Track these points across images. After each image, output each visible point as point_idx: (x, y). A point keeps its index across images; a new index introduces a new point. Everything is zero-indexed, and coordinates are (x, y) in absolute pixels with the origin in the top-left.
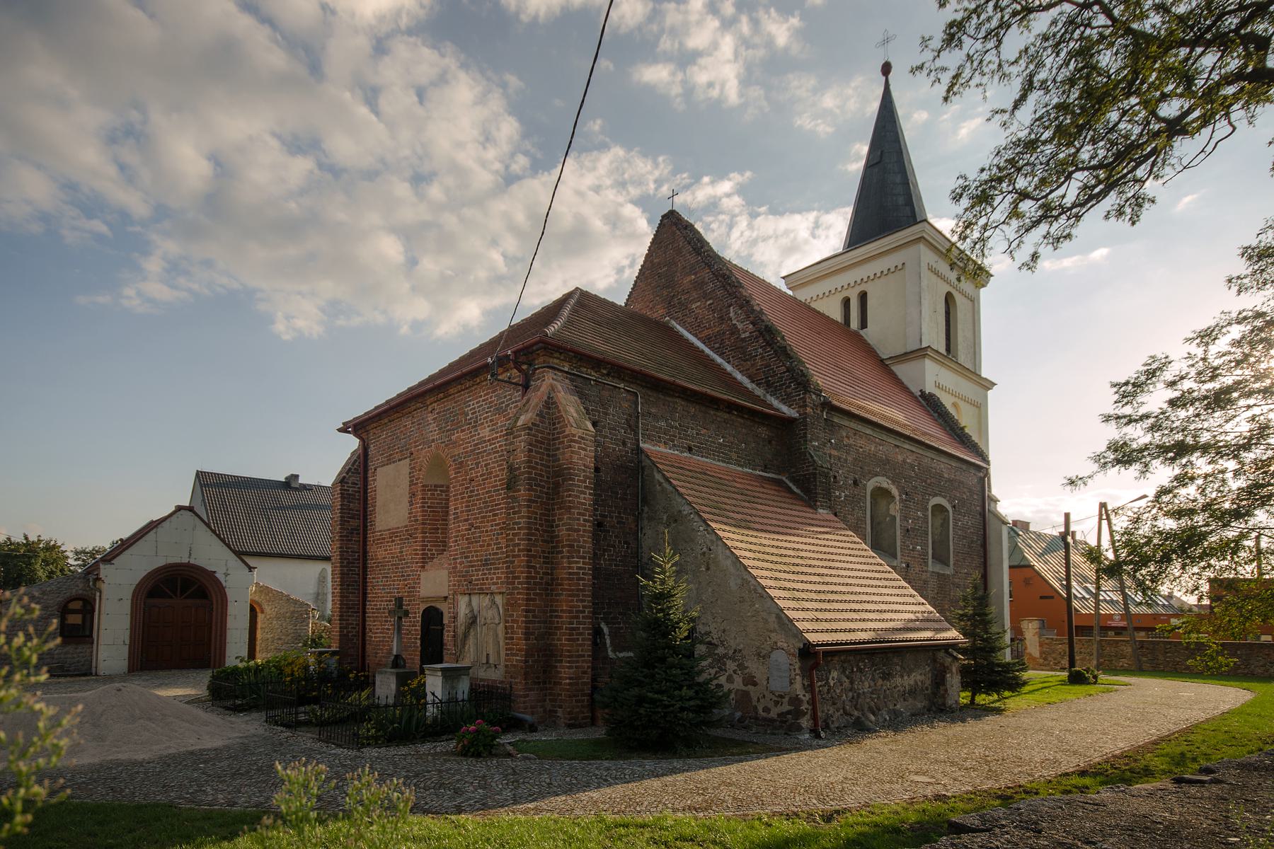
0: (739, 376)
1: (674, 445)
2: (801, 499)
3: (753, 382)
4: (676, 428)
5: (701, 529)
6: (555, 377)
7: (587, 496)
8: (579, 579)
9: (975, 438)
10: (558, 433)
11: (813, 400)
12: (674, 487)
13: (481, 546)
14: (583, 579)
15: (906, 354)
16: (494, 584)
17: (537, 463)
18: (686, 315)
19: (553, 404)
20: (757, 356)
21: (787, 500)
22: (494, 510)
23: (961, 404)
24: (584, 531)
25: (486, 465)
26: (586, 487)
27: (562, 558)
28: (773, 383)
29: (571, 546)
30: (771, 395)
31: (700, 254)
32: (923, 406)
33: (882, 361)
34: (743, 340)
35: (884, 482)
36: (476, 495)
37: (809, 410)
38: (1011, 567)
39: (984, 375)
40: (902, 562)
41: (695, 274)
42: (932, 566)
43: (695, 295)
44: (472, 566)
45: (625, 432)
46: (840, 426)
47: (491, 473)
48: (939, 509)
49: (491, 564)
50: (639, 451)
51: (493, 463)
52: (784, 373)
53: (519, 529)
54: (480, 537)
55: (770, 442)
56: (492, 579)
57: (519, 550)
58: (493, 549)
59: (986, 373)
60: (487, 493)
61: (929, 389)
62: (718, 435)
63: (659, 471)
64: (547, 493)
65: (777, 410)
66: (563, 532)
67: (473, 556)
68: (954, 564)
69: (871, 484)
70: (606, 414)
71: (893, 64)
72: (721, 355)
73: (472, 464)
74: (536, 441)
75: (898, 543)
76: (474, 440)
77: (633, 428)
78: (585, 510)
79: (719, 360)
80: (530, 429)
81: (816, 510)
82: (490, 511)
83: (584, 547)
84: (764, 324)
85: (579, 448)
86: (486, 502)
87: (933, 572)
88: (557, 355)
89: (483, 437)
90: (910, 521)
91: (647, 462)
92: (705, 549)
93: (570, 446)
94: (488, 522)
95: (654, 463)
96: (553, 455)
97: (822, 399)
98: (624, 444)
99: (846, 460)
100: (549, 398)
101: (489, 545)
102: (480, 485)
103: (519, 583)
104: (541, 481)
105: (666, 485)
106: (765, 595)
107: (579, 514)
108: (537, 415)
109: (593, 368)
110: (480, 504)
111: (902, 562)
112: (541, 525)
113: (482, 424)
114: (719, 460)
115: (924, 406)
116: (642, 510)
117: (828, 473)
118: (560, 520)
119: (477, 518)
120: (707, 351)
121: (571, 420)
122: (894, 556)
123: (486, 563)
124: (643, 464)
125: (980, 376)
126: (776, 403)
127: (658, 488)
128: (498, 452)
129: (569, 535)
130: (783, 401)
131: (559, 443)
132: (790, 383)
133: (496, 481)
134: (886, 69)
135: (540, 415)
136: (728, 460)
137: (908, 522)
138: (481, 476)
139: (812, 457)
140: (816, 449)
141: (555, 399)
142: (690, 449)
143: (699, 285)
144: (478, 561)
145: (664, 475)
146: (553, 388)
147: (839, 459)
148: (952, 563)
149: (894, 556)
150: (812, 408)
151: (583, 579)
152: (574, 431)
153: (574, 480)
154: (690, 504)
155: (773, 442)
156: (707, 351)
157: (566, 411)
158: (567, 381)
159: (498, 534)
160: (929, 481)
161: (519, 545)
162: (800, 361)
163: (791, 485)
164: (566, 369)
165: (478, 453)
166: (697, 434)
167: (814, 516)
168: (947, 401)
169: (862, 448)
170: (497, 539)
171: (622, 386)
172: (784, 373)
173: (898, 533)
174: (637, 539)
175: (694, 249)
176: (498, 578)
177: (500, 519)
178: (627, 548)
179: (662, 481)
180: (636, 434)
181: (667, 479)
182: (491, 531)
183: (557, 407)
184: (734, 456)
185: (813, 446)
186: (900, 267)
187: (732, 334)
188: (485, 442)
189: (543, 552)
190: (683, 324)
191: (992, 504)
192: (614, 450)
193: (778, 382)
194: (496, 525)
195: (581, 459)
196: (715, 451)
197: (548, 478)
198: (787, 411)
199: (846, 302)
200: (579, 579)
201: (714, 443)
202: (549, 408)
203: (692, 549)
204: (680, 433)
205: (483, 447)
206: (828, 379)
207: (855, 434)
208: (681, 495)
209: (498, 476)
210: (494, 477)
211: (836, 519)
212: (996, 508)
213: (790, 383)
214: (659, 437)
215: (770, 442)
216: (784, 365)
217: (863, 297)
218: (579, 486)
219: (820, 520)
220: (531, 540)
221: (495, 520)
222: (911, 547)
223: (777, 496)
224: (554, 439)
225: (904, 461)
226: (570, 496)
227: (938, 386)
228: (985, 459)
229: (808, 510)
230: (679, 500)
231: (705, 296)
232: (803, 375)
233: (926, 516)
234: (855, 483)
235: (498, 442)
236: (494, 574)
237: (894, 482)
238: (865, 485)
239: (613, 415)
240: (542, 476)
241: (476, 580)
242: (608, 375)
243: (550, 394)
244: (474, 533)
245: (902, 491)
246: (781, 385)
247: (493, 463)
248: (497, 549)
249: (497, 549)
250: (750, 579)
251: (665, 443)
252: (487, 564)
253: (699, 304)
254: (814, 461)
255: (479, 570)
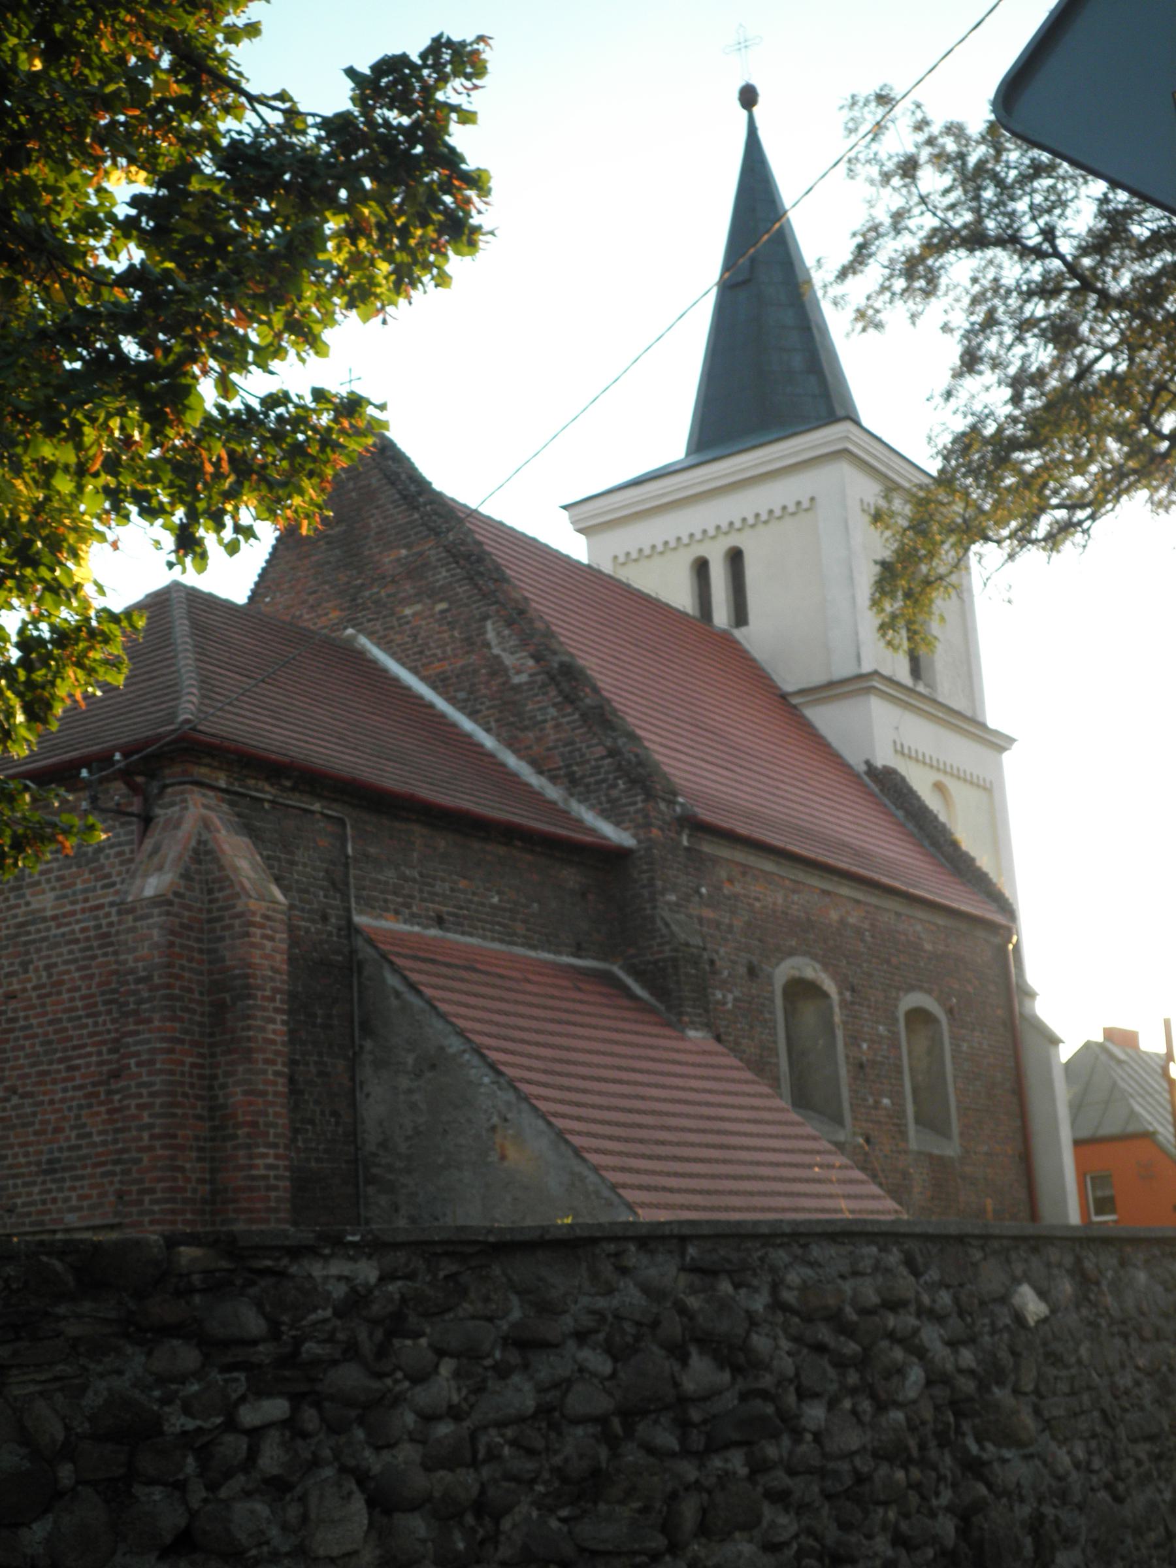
0: (511, 761)
1: (413, 915)
2: (652, 1010)
3: (541, 772)
4: (414, 880)
5: (486, 1080)
6: (205, 801)
7: (279, 1027)
8: (270, 1188)
9: (984, 862)
10: (220, 909)
11: (661, 812)
12: (429, 1002)
13: (36, 1133)
14: (276, 1188)
15: (831, 685)
16: (72, 1210)
17: (182, 968)
18: (392, 628)
19: (207, 853)
20: (545, 721)
21: (627, 1014)
22: (70, 1058)
23: (952, 785)
24: (276, 1094)
25: (48, 967)
26: (277, 1010)
27: (235, 1148)
28: (583, 777)
29: (254, 1124)
30: (580, 801)
31: (416, 508)
32: (872, 794)
33: (784, 697)
34: (517, 688)
35: (811, 970)
36: (23, 1028)
37: (655, 833)
38: (1077, 1143)
39: (991, 724)
40: (854, 1134)
41: (408, 546)
42: (915, 1138)
43: (408, 588)
44: (15, 1176)
45: (326, 896)
46: (715, 860)
47: (61, 983)
48: (919, 1016)
49: (64, 1169)
50: (351, 929)
51: (66, 962)
52: (602, 758)
53: (152, 1095)
54: (34, 1114)
55: (583, 895)
56: (67, 1200)
57: (153, 1137)
58: (68, 1139)
59: (994, 720)
60: (51, 1022)
61: (884, 758)
62: (489, 890)
63: (396, 970)
64: (200, 1024)
65: (592, 831)
66: (237, 1095)
67: (15, 1156)
68: (962, 1134)
69: (785, 971)
70: (292, 863)
71: (760, 90)
72: (472, 715)
73: (11, 964)
74: (182, 925)
75: (845, 1094)
76: (15, 916)
77: (338, 885)
78: (277, 1053)
79: (467, 725)
80: (170, 903)
81: (682, 1031)
82: (60, 1061)
83: (275, 1125)
84: (557, 658)
85: (265, 937)
86: (50, 1042)
87: (919, 1153)
88: (207, 760)
89: (39, 911)
90: (865, 1046)
91: (367, 952)
92: (495, 1120)
93: (247, 934)
94: (54, 1082)
95: (384, 956)
96: (209, 951)
97: (678, 809)
98: (325, 918)
99: (730, 926)
100: (199, 842)
101: (58, 1130)
102: (33, 1007)
103: (153, 1202)
104: (191, 1000)
105: (411, 997)
106: (616, 1200)
107: (267, 1061)
108: (182, 876)
109: (267, 779)
110: (33, 1045)
111: (854, 1134)
112: (192, 1086)
113: (38, 883)
114: (493, 939)
115: (872, 794)
116: (361, 1047)
117: (700, 956)
118: (227, 1074)
119: (28, 1076)
120: (441, 704)
121: (247, 885)
122: (839, 1121)
123: (51, 1168)
124: (360, 956)
125: (983, 726)
126: (590, 818)
127: (394, 1002)
128: (77, 941)
129: (250, 1103)
130: (605, 814)
131: (224, 928)
132: (616, 778)
133: (72, 999)
134: (748, 97)
135: (186, 876)
136: (508, 937)
137: (859, 1046)
138: (35, 988)
139: (667, 925)
140: (675, 907)
141: (211, 845)
142: (440, 921)
143: (415, 570)
144: (29, 1164)
145: (405, 979)
146: (206, 824)
147: (718, 925)
148: (955, 1129)
149: (839, 1121)
150: (661, 829)
151: (276, 1188)
152: (253, 905)
153: (254, 997)
154: (461, 1033)
155: (591, 897)
156: (441, 704)
157: (236, 869)
158: (225, 807)
159: (80, 1107)
160: (894, 960)
161: (150, 1126)
162: (633, 737)
163: (630, 981)
164: (222, 784)
165: (26, 943)
166: (452, 890)
167: (681, 1045)
168: (920, 782)
169: (757, 899)
170: (78, 1117)
171: (317, 807)
172: (602, 758)
173: (843, 1072)
174: (353, 1105)
175: (405, 497)
176: (81, 1198)
177: (84, 1076)
178: (337, 1124)
179: (402, 988)
180: (345, 898)
181: (413, 987)
182: (63, 1100)
183: (217, 860)
184: (520, 928)
185: (668, 903)
186: (806, 504)
187: (493, 674)
188: (44, 920)
189: (197, 1138)
190: (385, 644)
191: (1027, 1002)
192: (307, 931)
193: (592, 775)
194: (75, 1088)
195: (266, 957)
196: (485, 921)
197: (201, 994)
198: (611, 832)
199: (701, 568)
200: (270, 1188)
201: (483, 905)
202: (199, 862)
203: (469, 1121)
204: (421, 891)
205: (38, 931)
206: (683, 757)
207: (744, 874)
208: (442, 1016)
209: (78, 989)
210: (69, 991)
211: (719, 1048)
212: (1033, 1009)
213: (616, 778)
214: (386, 901)
215: (583, 895)
216: (601, 743)
217: (735, 558)
218: (264, 1009)
219: (691, 1052)
220: (174, 1115)
221: (73, 1079)
222: (871, 1101)
223: (608, 1006)
224: (210, 921)
225: (842, 921)
226: (249, 1028)
227: (900, 751)
228: (1007, 908)
229: (666, 1031)
230: (439, 1025)
231: (434, 594)
232: (640, 764)
233: (895, 1035)
234: (752, 971)
235: (78, 922)
236: (73, 1189)
237: (826, 967)
238: (770, 977)
239: (305, 865)
240: (191, 991)
241: (24, 1205)
242: (293, 789)
243: (200, 834)
244: (20, 1106)
245: (845, 984)
246: (597, 783)
247: (66, 962)
248: (79, 1137)
249: (79, 1137)
250: (586, 1172)
251: (397, 912)
252: (54, 1171)
253: (418, 607)
254: (672, 934)
255: (34, 1183)
